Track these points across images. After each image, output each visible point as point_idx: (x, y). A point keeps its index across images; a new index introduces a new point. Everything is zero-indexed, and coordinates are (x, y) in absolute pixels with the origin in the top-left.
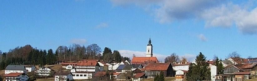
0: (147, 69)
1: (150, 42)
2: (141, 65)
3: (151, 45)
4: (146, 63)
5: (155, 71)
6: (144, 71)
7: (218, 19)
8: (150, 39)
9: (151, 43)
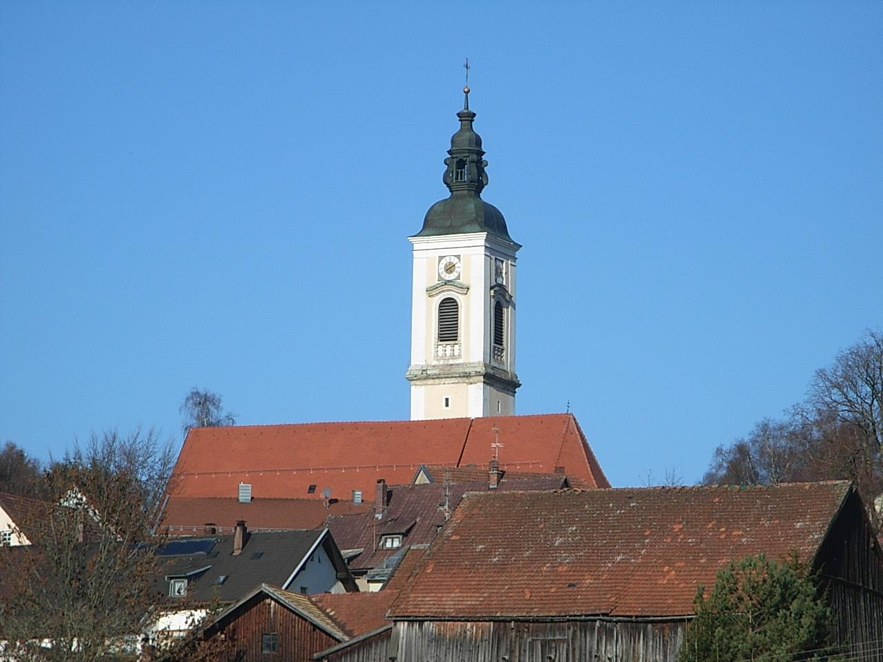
0: (427, 603)
1: (467, 165)
2: (329, 545)
3: (493, 223)
4: (400, 509)
5: (584, 624)
6: (387, 635)
7: (557, 542)
8: (467, 117)
9: (485, 195)
